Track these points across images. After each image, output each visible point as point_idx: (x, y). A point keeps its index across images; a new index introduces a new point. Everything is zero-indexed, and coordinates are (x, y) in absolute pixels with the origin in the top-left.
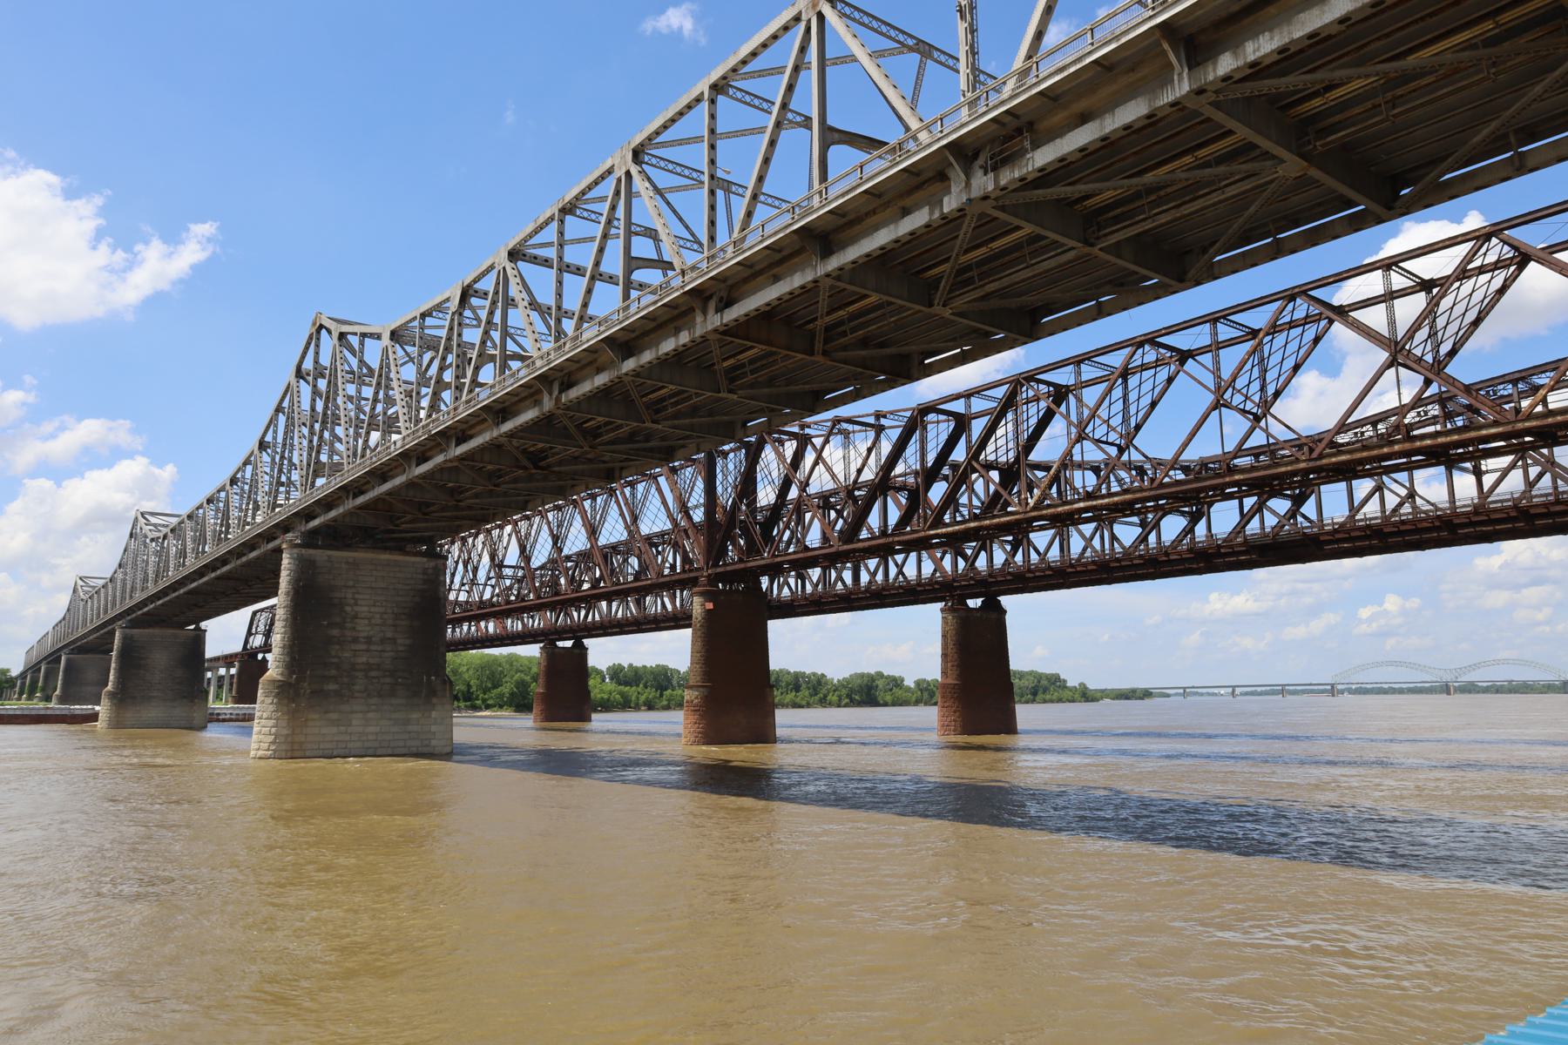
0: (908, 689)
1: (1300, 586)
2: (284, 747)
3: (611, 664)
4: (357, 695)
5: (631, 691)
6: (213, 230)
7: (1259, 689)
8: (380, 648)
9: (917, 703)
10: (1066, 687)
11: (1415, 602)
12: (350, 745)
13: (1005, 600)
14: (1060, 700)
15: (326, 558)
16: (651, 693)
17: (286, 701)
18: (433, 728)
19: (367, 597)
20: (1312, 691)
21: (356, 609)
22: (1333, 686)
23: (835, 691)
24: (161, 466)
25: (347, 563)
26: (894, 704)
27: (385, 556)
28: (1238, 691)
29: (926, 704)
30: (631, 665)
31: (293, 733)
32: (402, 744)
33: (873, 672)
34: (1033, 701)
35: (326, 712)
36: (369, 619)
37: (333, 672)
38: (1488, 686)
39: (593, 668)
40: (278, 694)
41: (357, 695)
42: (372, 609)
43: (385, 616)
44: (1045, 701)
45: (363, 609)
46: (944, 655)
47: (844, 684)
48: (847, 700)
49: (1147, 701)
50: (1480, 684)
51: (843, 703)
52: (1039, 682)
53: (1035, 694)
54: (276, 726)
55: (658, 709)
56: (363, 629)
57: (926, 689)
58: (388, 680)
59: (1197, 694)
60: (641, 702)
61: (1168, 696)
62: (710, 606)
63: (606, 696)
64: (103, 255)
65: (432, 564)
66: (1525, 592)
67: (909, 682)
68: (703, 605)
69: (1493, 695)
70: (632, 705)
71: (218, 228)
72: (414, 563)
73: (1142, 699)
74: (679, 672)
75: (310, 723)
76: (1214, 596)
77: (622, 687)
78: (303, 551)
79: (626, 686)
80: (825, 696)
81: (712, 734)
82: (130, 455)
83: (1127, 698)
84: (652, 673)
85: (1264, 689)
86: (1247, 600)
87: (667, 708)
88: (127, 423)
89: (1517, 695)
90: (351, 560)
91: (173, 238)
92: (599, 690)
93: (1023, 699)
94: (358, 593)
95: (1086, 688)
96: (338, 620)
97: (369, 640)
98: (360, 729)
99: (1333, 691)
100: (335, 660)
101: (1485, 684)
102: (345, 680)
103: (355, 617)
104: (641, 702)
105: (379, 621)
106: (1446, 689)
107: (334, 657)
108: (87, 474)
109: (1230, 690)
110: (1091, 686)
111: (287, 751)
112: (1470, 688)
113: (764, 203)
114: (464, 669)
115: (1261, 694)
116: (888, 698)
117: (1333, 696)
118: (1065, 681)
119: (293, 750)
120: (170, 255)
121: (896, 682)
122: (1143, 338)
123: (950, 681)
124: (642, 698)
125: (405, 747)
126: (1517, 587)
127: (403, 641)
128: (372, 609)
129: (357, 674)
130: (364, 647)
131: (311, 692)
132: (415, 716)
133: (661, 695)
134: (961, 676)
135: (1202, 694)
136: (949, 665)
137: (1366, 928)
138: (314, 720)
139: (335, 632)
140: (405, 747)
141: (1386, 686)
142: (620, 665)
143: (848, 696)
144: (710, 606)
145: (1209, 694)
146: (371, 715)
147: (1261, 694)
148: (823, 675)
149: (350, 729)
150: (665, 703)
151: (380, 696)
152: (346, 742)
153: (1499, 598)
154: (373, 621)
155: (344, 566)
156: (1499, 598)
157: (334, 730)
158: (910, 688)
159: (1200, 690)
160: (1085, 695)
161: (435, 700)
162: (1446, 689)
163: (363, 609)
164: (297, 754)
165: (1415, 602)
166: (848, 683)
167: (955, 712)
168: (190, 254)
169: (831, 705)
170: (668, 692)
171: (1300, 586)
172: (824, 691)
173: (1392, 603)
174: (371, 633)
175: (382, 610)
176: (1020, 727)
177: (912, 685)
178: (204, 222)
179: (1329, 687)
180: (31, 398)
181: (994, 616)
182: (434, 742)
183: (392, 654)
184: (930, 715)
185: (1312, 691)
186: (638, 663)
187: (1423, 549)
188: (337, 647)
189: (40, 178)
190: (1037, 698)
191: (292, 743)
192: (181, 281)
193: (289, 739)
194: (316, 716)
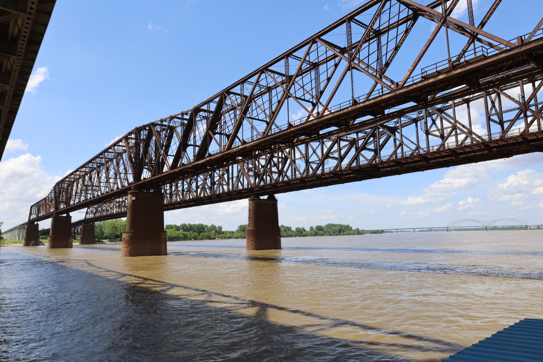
0: (293, 231)
1: (439, 194)
3: (182, 224)
6: (46, 70)
7: (424, 229)
9: (296, 236)
10: (352, 230)
11: (478, 199)
13: (277, 196)
14: (349, 234)
16: (196, 234)
20: (442, 230)
22: (447, 228)
24: (36, 157)
26: (287, 237)
28: (417, 230)
29: (299, 236)
30: (189, 224)
34: (339, 235)
38: (501, 228)
39: (283, 226)
44: (343, 235)
46: (249, 218)
49: (383, 234)
50: (498, 227)
52: (341, 228)
53: (340, 232)
57: (299, 231)
59: (403, 231)
61: (392, 232)
62: (134, 198)
63: (176, 236)
66: (515, 195)
67: (294, 229)
68: (131, 198)
69: (502, 231)
70: (189, 238)
71: (48, 69)
73: (381, 233)
74: (208, 226)
76: (410, 198)
77: (184, 232)
79: (186, 231)
81: (258, 247)
82: (24, 153)
83: (376, 233)
84: (197, 227)
85: (426, 229)
86: (421, 199)
87: (202, 239)
88: (20, 140)
89: (510, 231)
92: (169, 233)
93: (335, 234)
95: (358, 229)
99: (448, 230)
101: (500, 227)
104: (192, 237)
106: (486, 229)
108: (10, 160)
109: (396, 230)
110: (361, 229)
112: (495, 228)
114: (119, 226)
115: (425, 231)
116: (285, 234)
117: (448, 231)
118: (351, 227)
121: (289, 229)
122: (263, 68)
123: (251, 228)
124: (192, 236)
126: (513, 194)
133: (200, 234)
134: (255, 226)
135: (405, 231)
136: (251, 222)
137: (326, 350)
141: (467, 228)
142: (185, 224)
144: (134, 198)
145: (407, 231)
147: (425, 231)
150: (201, 237)
153: (506, 197)
156: (506, 197)
158: (293, 231)
159: (404, 230)
160: (359, 232)
162: (486, 229)
165: (478, 199)
167: (252, 241)
170: (202, 234)
171: (439, 194)
173: (470, 200)
176: (282, 246)
177: (294, 230)
178: (42, 67)
179: (446, 228)
181: (272, 202)
184: (243, 242)
185: (442, 230)
186: (192, 223)
187: (423, 171)
190: (340, 234)
192: (36, 88)
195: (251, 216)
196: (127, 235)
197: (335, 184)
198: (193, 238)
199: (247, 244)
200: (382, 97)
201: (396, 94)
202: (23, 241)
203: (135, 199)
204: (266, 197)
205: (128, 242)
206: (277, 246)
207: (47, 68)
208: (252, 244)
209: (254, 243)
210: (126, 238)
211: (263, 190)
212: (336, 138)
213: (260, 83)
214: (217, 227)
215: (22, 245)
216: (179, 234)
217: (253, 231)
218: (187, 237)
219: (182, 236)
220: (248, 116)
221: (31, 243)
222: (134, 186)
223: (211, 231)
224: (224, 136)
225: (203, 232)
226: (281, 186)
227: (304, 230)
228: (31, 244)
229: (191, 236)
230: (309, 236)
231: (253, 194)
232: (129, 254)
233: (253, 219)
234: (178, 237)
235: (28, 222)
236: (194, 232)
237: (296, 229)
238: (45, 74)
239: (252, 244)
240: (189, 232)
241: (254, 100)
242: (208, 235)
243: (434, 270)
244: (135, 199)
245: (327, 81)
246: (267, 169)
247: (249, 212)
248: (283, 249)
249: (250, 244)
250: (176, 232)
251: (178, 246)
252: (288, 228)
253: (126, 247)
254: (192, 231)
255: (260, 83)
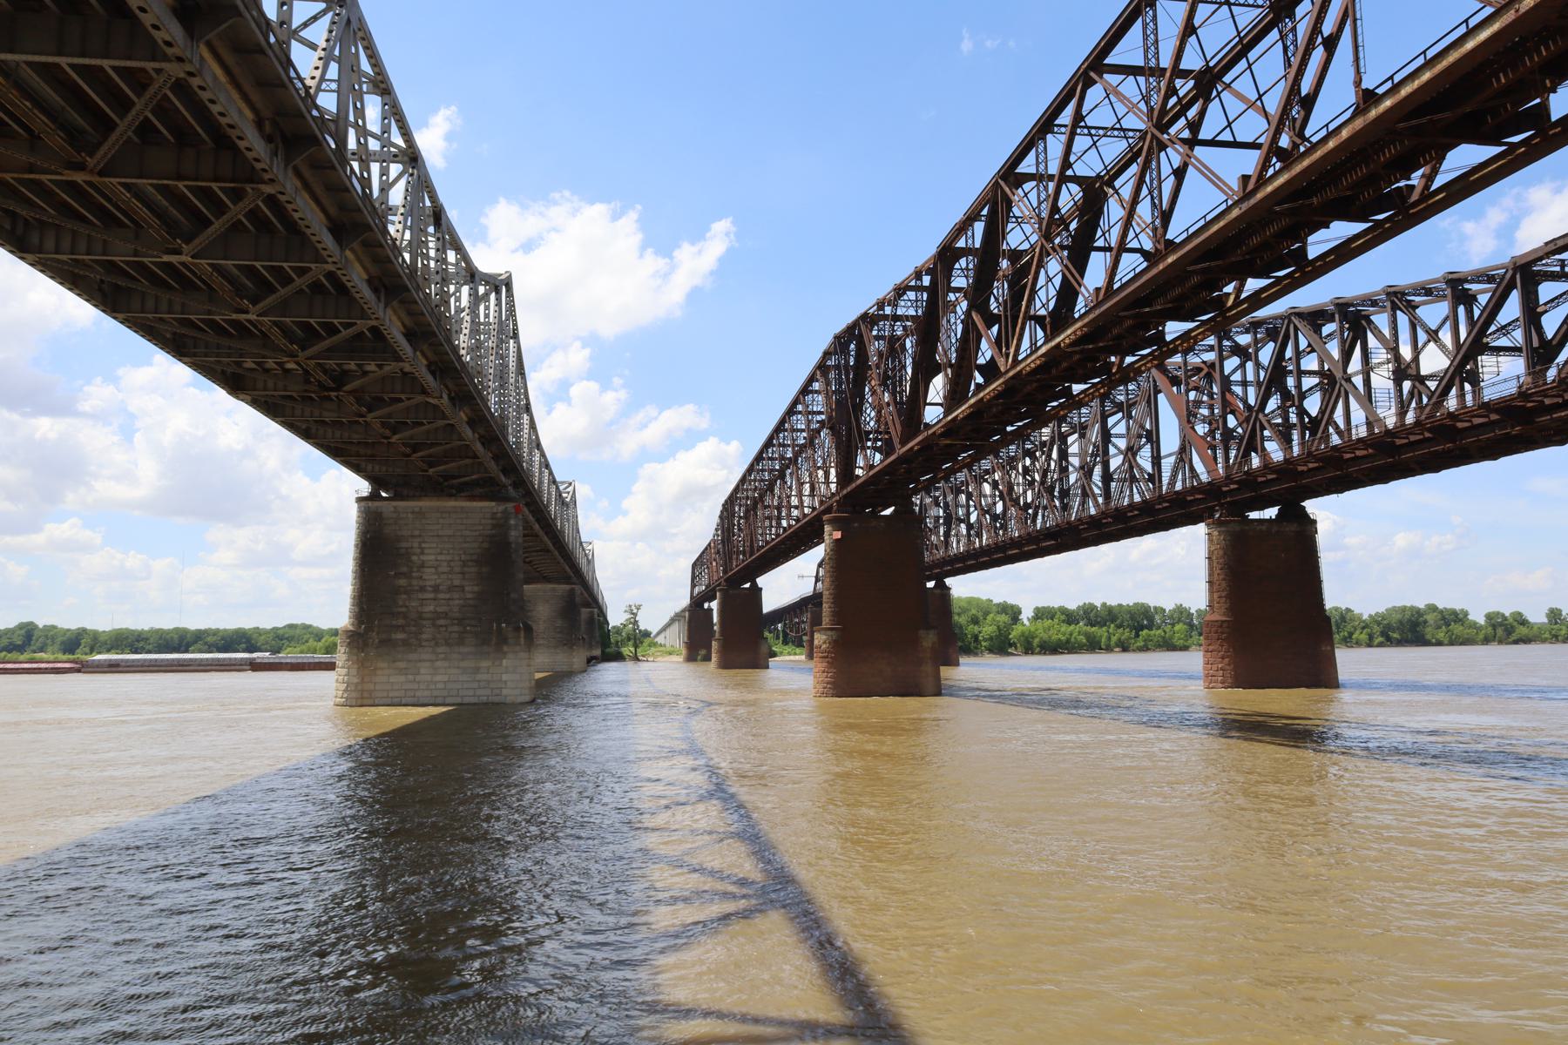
0: (1474, 625)
2: (354, 695)
3: (1081, 604)
4: (424, 644)
5: (1101, 632)
6: (728, 225)
8: (447, 596)
9: (1486, 641)
12: (419, 694)
13: (1312, 506)
15: (392, 509)
16: (1126, 634)
17: (355, 651)
18: (505, 677)
19: (435, 545)
21: (422, 557)
23: (1363, 628)
25: (413, 513)
26: (1451, 643)
27: (451, 503)
29: (1500, 642)
30: (1104, 605)
31: (362, 681)
32: (471, 693)
33: (1152, 605)
35: (394, 661)
36: (436, 568)
37: (401, 622)
40: (349, 643)
41: (424, 644)
42: (439, 558)
43: (452, 564)
45: (429, 558)
47: (1377, 620)
48: (1381, 639)
51: (1376, 642)
54: (347, 675)
55: (1134, 651)
56: (430, 577)
57: (1501, 624)
58: (456, 628)
60: (1112, 643)
62: (838, 535)
64: (653, 263)
65: (501, 508)
70: (1103, 647)
71: (733, 223)
72: (481, 508)
75: (379, 672)
77: (1088, 628)
78: (370, 504)
79: (1092, 625)
80: (1351, 634)
81: (1246, 675)
82: (702, 436)
84: (1130, 612)
87: (1145, 649)
88: (690, 407)
90: (417, 510)
91: (698, 235)
94: (424, 542)
96: (404, 569)
97: (436, 589)
98: (429, 678)
100: (404, 609)
102: (413, 629)
103: (422, 566)
104: (1112, 643)
105: (446, 569)
107: (401, 607)
108: (678, 456)
111: (357, 699)
113: (1158, 59)
116: (1441, 635)
119: (362, 698)
120: (700, 252)
121: (1457, 617)
123: (1217, 617)
124: (1114, 639)
125: (388, 697)
127: (471, 589)
128: (439, 558)
129: (424, 622)
130: (431, 596)
131: (380, 642)
132: (485, 664)
133: (1137, 635)
136: (1216, 595)
138: (382, 669)
139: (402, 582)
140: (388, 697)
143: (1383, 634)
144: (838, 535)
146: (439, 664)
148: (1348, 610)
149: (418, 678)
150: (1140, 643)
151: (448, 644)
152: (416, 690)
154: (440, 569)
155: (410, 515)
157: (402, 678)
158: (1475, 623)
161: (505, 648)
163: (429, 558)
164: (366, 702)
166: (1383, 619)
167: (1223, 658)
168: (715, 246)
169: (1358, 644)
170: (1145, 632)
172: (1349, 628)
174: (438, 581)
175: (449, 558)
177: (1481, 621)
180: (622, 394)
181: (1291, 528)
182: (505, 692)
183: (461, 602)
184: (1194, 660)
188: (404, 596)
189: (599, 210)
191: (363, 691)
192: (712, 273)
193: (359, 688)
194: (385, 665)
195: (1216, 576)
196: (824, 637)
197: (1527, 450)
198: (1117, 646)
199: (1205, 669)
200: (1462, 46)
201: (1522, 11)
202: (684, 652)
203: (839, 537)
204: (1271, 513)
205: (827, 657)
206: (1323, 676)
207: (730, 219)
208: (1221, 669)
209: (1229, 665)
210: (824, 646)
211: (1253, 489)
212: (1510, 273)
213: (1090, 121)
214: (1193, 611)
215: (680, 659)
216: (1071, 635)
217: (1225, 625)
218: (1099, 642)
219: (1083, 639)
220: (1100, 243)
221: (698, 654)
222: (836, 501)
223: (1173, 625)
224: (1033, 322)
225: (1150, 627)
226: (1310, 470)
227: (1524, 622)
228: (699, 657)
229: (1109, 639)
230: (1544, 641)
231: (1221, 505)
232: (834, 689)
233: (1224, 584)
234: (1068, 641)
235: (691, 605)
236: (1118, 627)
237: (1489, 617)
238: (727, 234)
239: (1221, 669)
240: (1104, 629)
241: (1114, 188)
242: (1164, 638)
243: (685, 900)
244: (839, 537)
245: (1326, 49)
246: (1261, 416)
247: (1209, 564)
248: (1344, 686)
249: (1215, 667)
250: (1064, 628)
251: (1083, 670)
252: (1454, 613)
253: (824, 672)
254: (1112, 625)
255: (1090, 121)
